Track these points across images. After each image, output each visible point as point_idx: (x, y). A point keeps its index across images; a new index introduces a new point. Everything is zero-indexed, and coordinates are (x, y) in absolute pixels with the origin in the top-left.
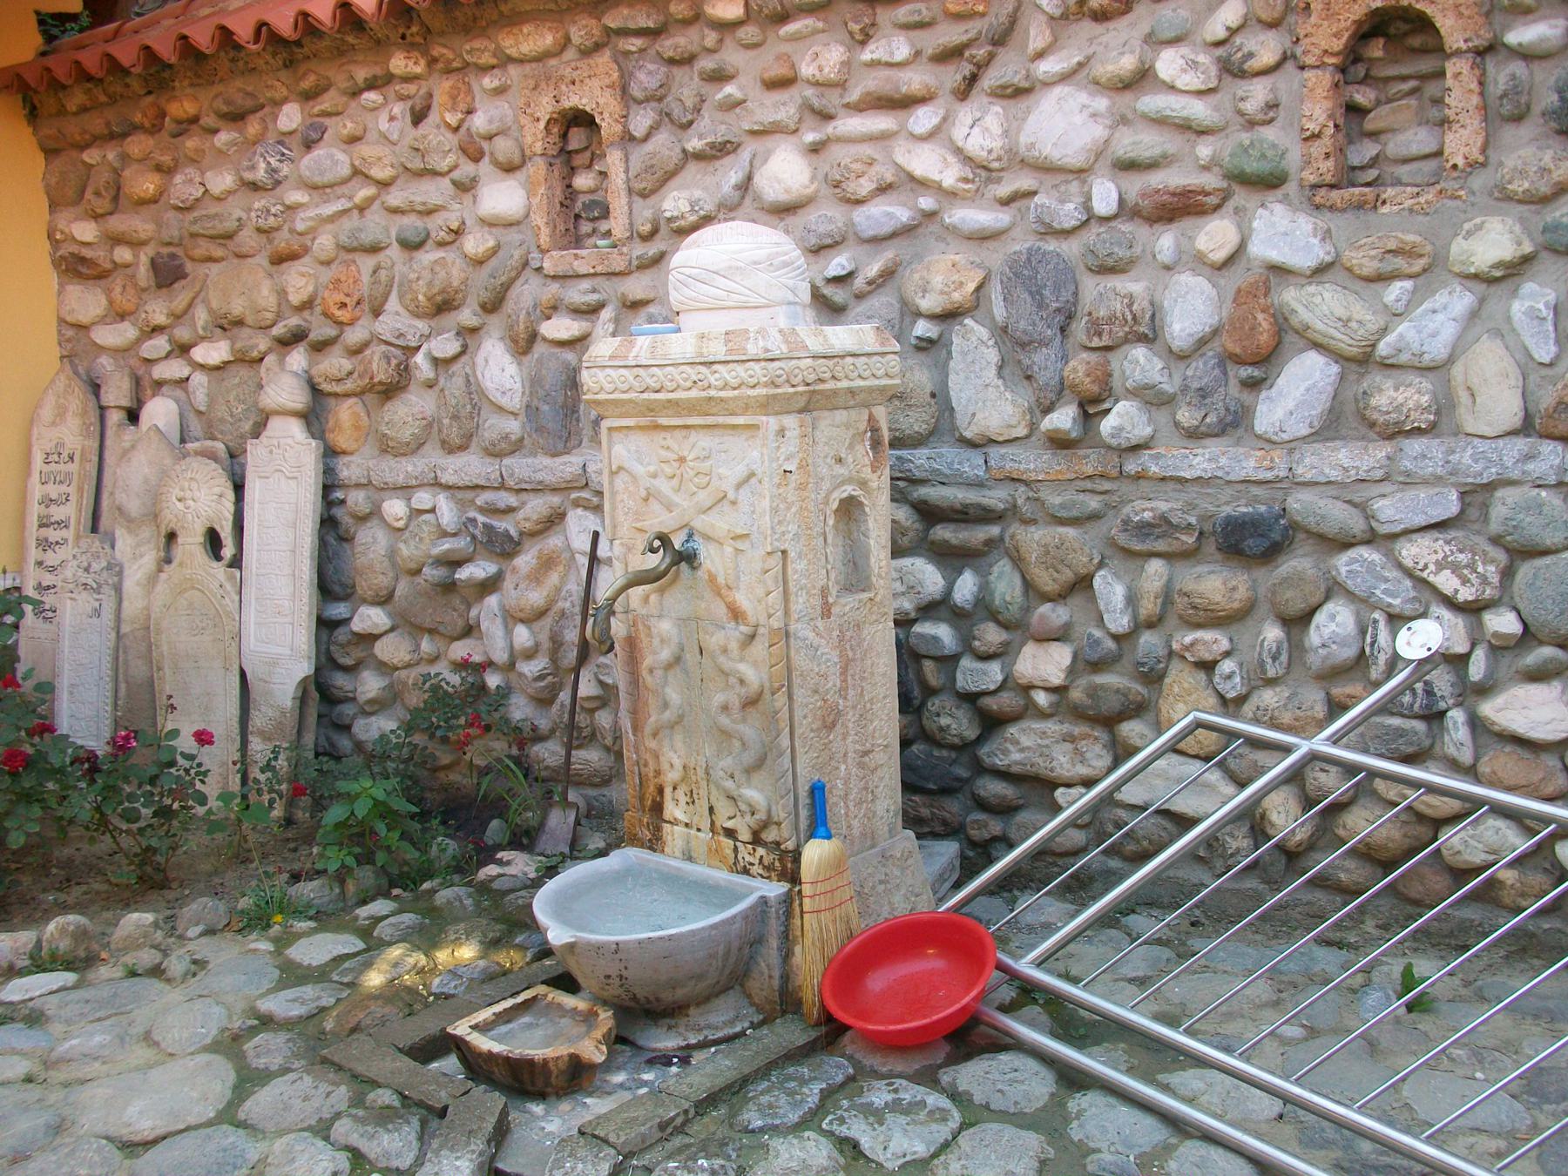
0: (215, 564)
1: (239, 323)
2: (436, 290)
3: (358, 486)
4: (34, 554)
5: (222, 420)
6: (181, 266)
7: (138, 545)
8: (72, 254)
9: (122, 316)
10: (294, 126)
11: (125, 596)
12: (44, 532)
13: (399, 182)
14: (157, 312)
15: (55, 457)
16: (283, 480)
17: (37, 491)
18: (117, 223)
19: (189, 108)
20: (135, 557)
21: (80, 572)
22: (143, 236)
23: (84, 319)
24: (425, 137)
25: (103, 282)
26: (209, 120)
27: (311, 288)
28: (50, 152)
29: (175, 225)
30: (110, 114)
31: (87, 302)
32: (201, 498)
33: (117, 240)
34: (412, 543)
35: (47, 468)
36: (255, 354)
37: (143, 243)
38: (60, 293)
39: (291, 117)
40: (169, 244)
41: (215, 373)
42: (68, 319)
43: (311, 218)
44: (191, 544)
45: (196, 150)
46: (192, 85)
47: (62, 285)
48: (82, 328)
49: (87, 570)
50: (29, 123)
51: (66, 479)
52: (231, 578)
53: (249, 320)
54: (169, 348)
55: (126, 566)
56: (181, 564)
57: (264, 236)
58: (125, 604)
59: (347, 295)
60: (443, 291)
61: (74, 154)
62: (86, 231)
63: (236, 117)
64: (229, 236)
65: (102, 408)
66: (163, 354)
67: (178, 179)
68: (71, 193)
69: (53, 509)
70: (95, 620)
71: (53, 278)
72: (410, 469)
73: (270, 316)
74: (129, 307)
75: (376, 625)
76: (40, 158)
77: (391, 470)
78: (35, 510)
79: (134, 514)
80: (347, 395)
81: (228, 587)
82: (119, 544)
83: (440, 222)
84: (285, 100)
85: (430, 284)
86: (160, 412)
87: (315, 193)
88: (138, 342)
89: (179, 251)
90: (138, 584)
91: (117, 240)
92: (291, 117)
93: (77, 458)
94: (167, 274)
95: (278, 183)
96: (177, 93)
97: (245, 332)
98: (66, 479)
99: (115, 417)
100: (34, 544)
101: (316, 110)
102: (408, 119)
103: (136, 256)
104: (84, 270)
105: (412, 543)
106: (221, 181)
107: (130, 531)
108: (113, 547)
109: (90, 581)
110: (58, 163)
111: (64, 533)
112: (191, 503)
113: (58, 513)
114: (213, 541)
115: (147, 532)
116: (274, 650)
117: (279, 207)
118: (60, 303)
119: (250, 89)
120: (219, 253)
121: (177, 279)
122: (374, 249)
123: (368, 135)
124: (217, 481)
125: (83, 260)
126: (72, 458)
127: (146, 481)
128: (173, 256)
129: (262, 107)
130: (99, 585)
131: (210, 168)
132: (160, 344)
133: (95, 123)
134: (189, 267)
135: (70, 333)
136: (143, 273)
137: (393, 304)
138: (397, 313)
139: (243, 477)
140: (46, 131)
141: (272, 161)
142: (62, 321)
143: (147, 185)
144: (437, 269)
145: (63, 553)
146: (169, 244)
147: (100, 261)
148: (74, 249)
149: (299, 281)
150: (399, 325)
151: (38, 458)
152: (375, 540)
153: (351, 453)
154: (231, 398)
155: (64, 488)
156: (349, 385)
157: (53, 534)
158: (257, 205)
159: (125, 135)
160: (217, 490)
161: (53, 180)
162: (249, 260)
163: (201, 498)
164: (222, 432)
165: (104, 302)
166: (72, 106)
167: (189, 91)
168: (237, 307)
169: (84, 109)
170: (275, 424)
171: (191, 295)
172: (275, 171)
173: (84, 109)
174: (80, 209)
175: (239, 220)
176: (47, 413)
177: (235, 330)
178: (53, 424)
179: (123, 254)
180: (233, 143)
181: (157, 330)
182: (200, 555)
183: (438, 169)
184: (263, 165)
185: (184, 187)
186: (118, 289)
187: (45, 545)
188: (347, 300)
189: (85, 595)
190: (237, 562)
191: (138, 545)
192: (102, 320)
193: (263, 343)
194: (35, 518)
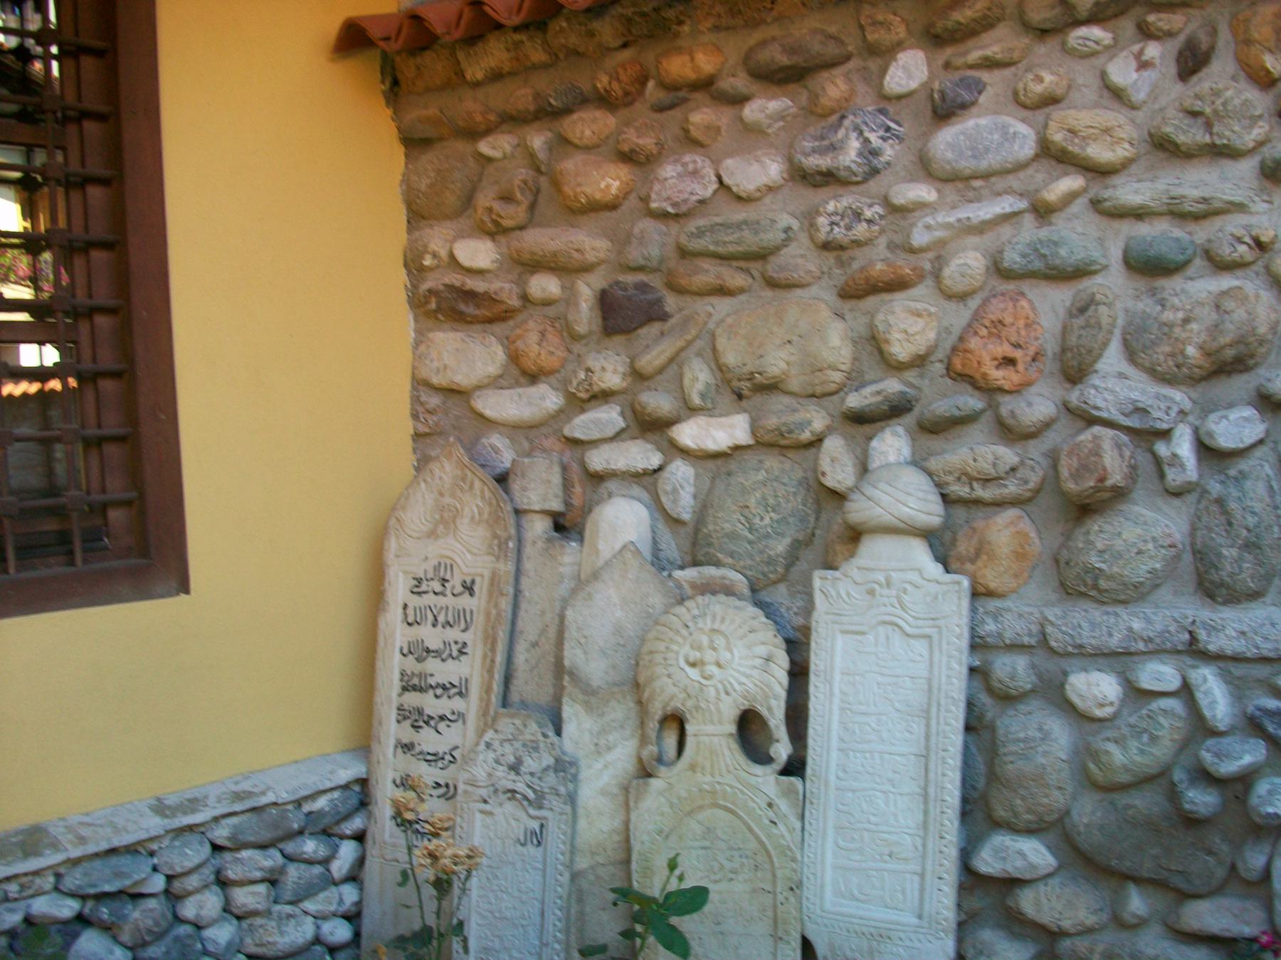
0: (758, 769)
1: (772, 387)
2: (1227, 339)
3: (1015, 647)
4: (391, 730)
5: (733, 536)
6: (659, 301)
7: (603, 731)
8: (450, 287)
9: (533, 378)
10: (914, 85)
11: (581, 811)
12: (412, 699)
13: (1134, 168)
14: (609, 369)
15: (437, 586)
16: (897, 639)
17: (395, 632)
18: (540, 240)
19: (706, 63)
20: (598, 751)
21: (501, 772)
22: (591, 257)
23: (462, 378)
24: (1216, 93)
25: (498, 328)
26: (738, 82)
27: (932, 335)
28: (414, 143)
29: (654, 241)
30: (542, 82)
31: (470, 357)
32: (730, 660)
33: (535, 265)
34: (1133, 744)
35: (415, 601)
36: (806, 436)
37: (586, 269)
38: (417, 344)
39: (909, 70)
40: (640, 269)
41: (711, 464)
42: (435, 380)
43: (948, 226)
44: (713, 733)
45: (708, 128)
46: (716, 28)
47: (421, 337)
48: (454, 392)
49: (515, 768)
50: (388, 104)
51: (462, 619)
52: (789, 792)
53: (794, 384)
54: (623, 425)
55: (583, 763)
56: (693, 767)
57: (830, 257)
58: (582, 823)
59: (1017, 346)
60: (1240, 341)
61: (460, 146)
62: (478, 253)
63: (788, 76)
64: (761, 256)
65: (518, 512)
66: (610, 432)
67: (669, 171)
68: (451, 200)
69: (432, 665)
70: (531, 849)
71: (405, 321)
72: (1137, 625)
73: (837, 377)
74: (547, 361)
75: (1033, 867)
76: (399, 151)
77: (1093, 625)
78: (392, 667)
79: (595, 683)
80: (1000, 504)
81: (783, 805)
82: (569, 728)
83: (1230, 229)
84: (899, 46)
85: (1216, 328)
86: (622, 521)
87: (949, 189)
88: (561, 415)
89: (656, 281)
90: (603, 792)
91: (535, 265)
92: (909, 70)
93: (481, 588)
94: (623, 314)
95: (875, 172)
96: (680, 42)
97: (779, 402)
98: (462, 619)
99: (539, 527)
100: (394, 715)
101: (974, 56)
102: (1173, 69)
103: (569, 290)
104: (470, 310)
105: (1133, 744)
106: (758, 171)
107: (588, 707)
108: (558, 732)
109: (520, 787)
110: (429, 160)
111: (458, 704)
112: (712, 669)
113: (441, 671)
114: (749, 728)
115: (621, 710)
116: (878, 914)
117: (878, 209)
118: (418, 357)
119: (832, 30)
120: (738, 280)
121: (650, 320)
122: (1079, 272)
123: (1075, 96)
124: (760, 636)
125: (470, 295)
126: (469, 588)
127: (618, 630)
128: (643, 287)
129: (848, 58)
130: (540, 796)
131: (730, 154)
132: (609, 417)
133: (521, 96)
134: (671, 302)
135: (434, 401)
136: (585, 313)
137: (1112, 359)
138: (1122, 376)
139: (806, 631)
140: (413, 114)
141: (873, 137)
142: (420, 384)
143: (609, 181)
144: (1229, 304)
145: (447, 739)
146: (640, 269)
147: (504, 296)
148: (455, 279)
149: (911, 324)
150: (1135, 395)
151: (398, 589)
152: (1046, 736)
153: (1001, 596)
154: (752, 502)
155: (453, 634)
156: (1012, 488)
157: (431, 704)
158: (831, 207)
159: (567, 111)
160: (762, 650)
161: (423, 184)
162: (798, 292)
163: (730, 660)
164: (732, 555)
165: (500, 354)
166: (475, 71)
167: (708, 38)
168: (777, 362)
169: (496, 76)
170: (875, 551)
171: (680, 343)
172: (875, 153)
173: (496, 76)
174: (463, 223)
175: (788, 230)
176: (417, 515)
177: (758, 399)
178: (432, 534)
179: (545, 285)
180: (781, 116)
181: (604, 396)
182: (731, 754)
183: (1238, 143)
184: (854, 144)
185: (677, 180)
186: (533, 338)
187: (418, 719)
188: (1018, 354)
189: (510, 807)
190: (795, 767)
191: (603, 731)
192: (495, 383)
193: (818, 420)
194: (396, 676)
